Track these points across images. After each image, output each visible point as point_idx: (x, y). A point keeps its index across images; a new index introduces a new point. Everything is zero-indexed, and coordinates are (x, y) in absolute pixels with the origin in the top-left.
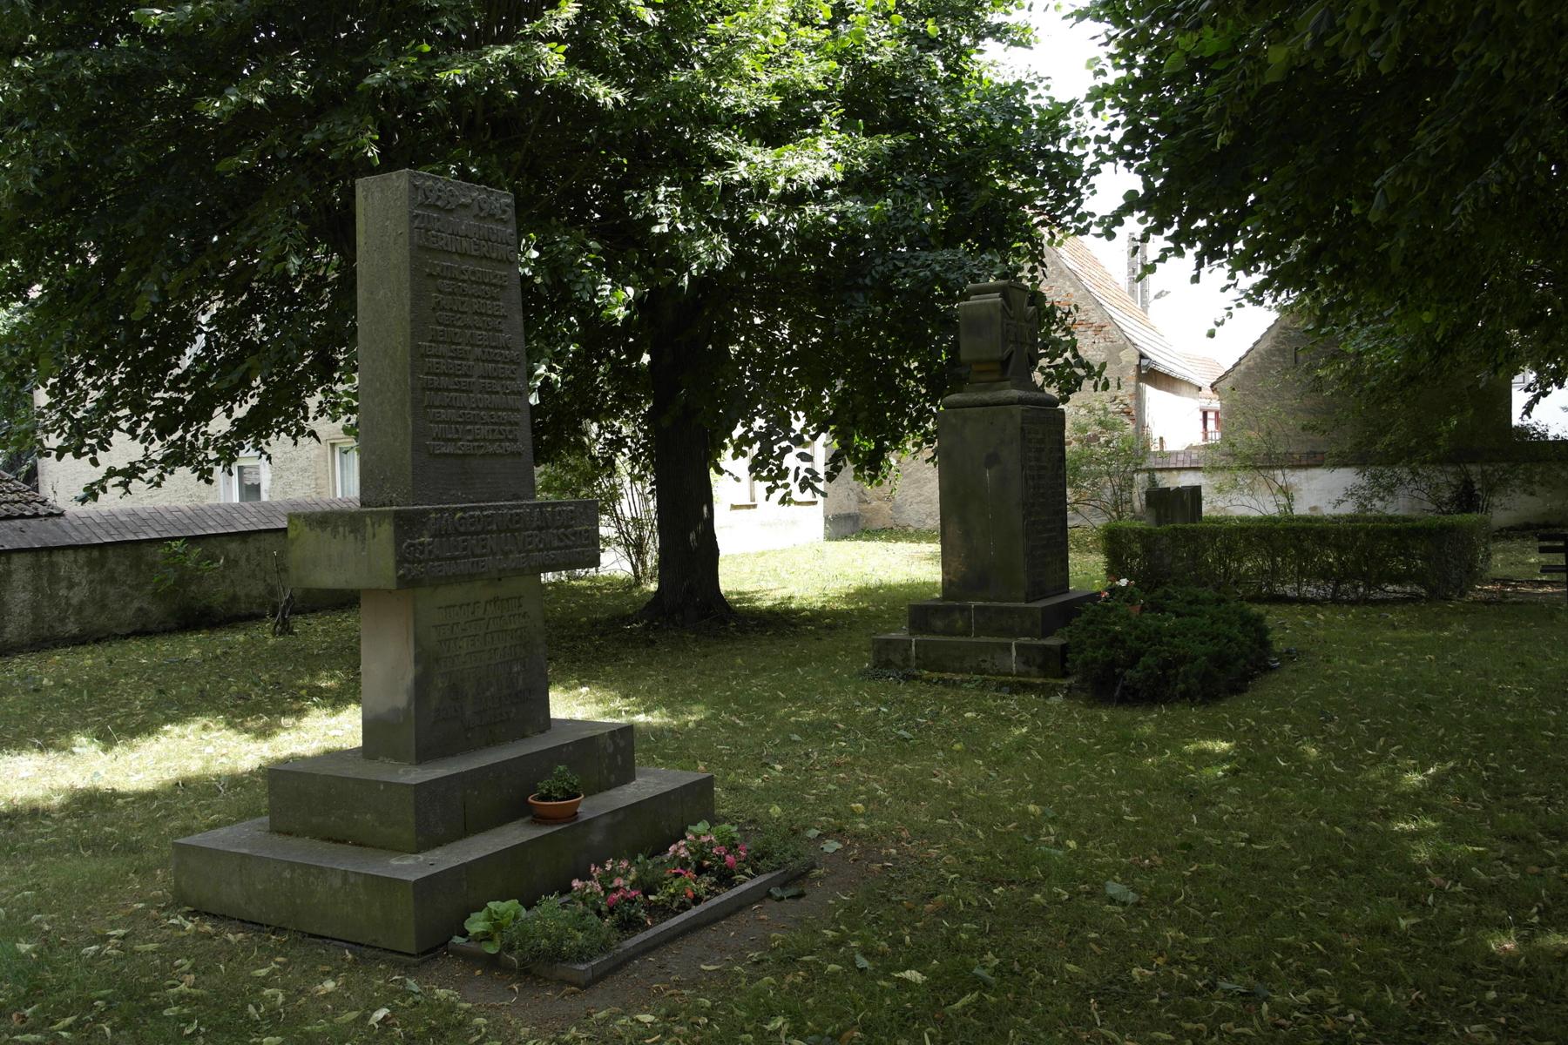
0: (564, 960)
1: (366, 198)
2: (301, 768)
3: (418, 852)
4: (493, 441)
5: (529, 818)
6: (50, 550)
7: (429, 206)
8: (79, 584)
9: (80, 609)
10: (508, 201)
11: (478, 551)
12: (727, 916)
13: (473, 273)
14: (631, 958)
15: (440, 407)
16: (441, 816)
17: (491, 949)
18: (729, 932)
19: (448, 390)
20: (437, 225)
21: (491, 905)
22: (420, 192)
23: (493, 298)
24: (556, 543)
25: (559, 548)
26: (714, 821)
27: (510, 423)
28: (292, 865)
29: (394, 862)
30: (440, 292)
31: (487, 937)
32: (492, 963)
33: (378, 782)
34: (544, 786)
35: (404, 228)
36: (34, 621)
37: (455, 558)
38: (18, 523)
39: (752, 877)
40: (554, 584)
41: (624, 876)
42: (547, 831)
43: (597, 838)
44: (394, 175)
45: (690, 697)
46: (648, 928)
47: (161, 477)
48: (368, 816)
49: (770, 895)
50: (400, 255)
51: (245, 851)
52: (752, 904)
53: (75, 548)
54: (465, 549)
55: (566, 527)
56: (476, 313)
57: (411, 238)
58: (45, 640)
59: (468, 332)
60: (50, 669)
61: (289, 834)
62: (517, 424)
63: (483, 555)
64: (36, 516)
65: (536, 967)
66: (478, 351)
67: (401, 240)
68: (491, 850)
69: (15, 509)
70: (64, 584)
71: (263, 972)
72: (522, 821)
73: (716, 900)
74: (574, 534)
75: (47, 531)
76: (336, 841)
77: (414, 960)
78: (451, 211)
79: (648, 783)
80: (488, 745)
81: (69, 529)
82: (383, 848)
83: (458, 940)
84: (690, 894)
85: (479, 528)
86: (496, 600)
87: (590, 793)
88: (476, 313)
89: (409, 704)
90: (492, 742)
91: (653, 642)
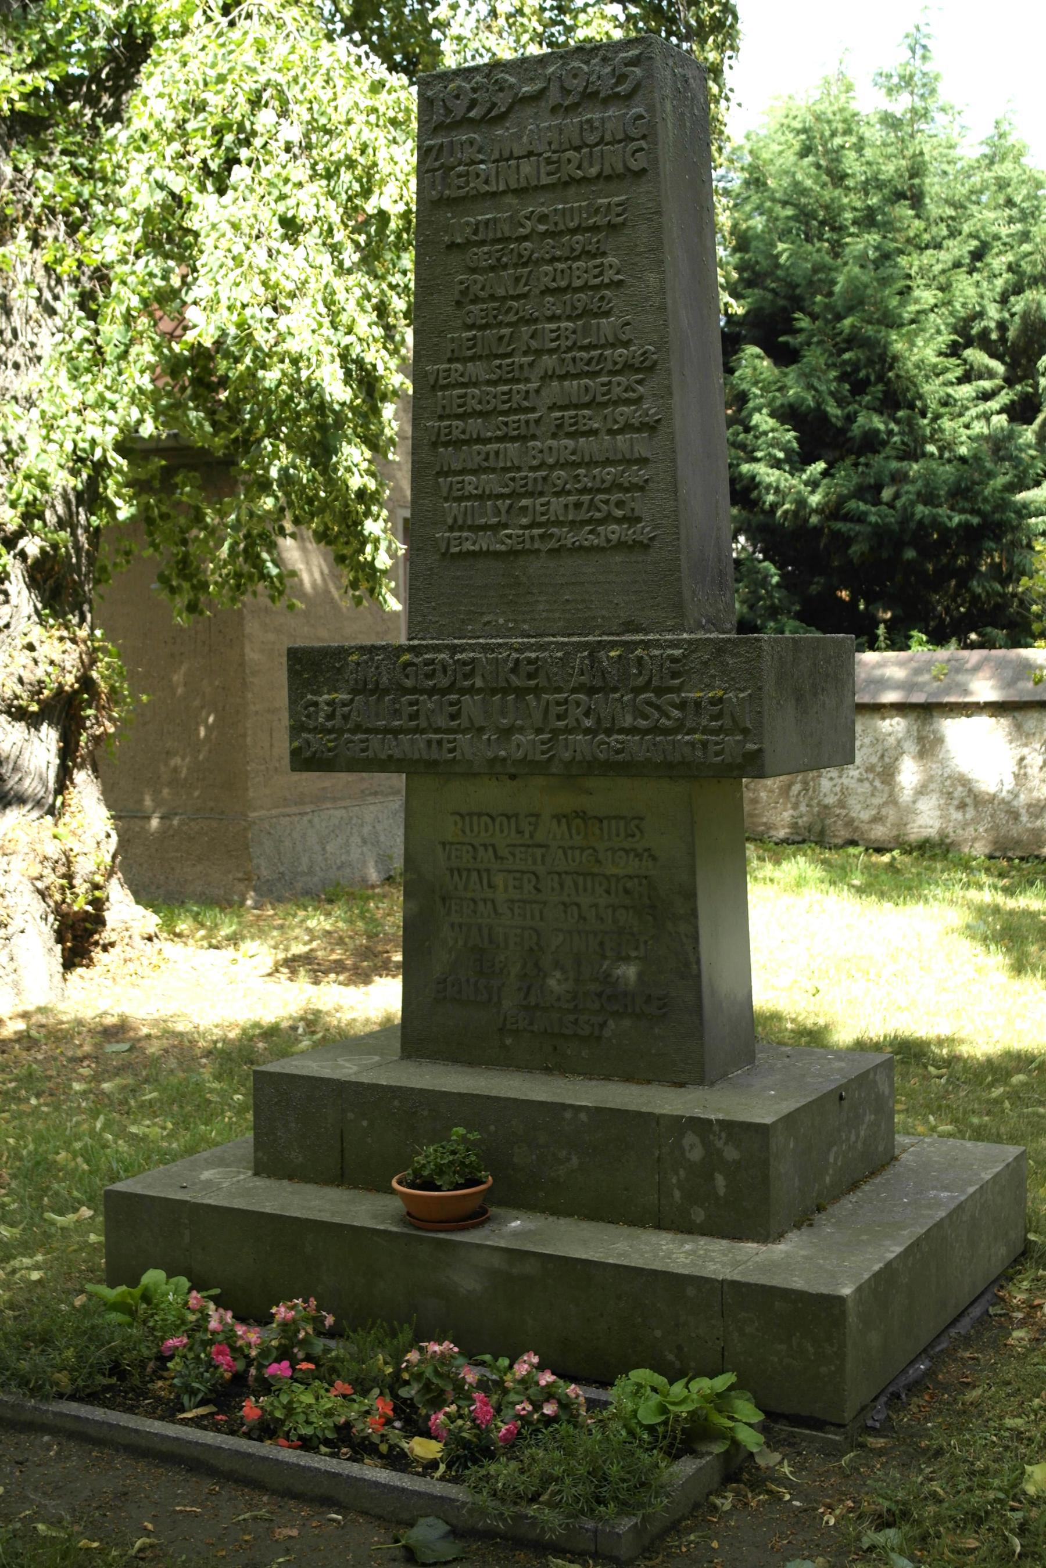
13: (543, 218)
15: (462, 472)
19: (480, 440)
23: (587, 254)
24: (628, 721)
25: (632, 731)
29: (622, 1246)
37: (396, 732)
54: (414, 716)
55: (660, 691)
56: (547, 291)
66: (548, 362)
74: (682, 706)
80: (547, 1070)
85: (445, 682)
88: (547, 291)
90: (556, 1065)
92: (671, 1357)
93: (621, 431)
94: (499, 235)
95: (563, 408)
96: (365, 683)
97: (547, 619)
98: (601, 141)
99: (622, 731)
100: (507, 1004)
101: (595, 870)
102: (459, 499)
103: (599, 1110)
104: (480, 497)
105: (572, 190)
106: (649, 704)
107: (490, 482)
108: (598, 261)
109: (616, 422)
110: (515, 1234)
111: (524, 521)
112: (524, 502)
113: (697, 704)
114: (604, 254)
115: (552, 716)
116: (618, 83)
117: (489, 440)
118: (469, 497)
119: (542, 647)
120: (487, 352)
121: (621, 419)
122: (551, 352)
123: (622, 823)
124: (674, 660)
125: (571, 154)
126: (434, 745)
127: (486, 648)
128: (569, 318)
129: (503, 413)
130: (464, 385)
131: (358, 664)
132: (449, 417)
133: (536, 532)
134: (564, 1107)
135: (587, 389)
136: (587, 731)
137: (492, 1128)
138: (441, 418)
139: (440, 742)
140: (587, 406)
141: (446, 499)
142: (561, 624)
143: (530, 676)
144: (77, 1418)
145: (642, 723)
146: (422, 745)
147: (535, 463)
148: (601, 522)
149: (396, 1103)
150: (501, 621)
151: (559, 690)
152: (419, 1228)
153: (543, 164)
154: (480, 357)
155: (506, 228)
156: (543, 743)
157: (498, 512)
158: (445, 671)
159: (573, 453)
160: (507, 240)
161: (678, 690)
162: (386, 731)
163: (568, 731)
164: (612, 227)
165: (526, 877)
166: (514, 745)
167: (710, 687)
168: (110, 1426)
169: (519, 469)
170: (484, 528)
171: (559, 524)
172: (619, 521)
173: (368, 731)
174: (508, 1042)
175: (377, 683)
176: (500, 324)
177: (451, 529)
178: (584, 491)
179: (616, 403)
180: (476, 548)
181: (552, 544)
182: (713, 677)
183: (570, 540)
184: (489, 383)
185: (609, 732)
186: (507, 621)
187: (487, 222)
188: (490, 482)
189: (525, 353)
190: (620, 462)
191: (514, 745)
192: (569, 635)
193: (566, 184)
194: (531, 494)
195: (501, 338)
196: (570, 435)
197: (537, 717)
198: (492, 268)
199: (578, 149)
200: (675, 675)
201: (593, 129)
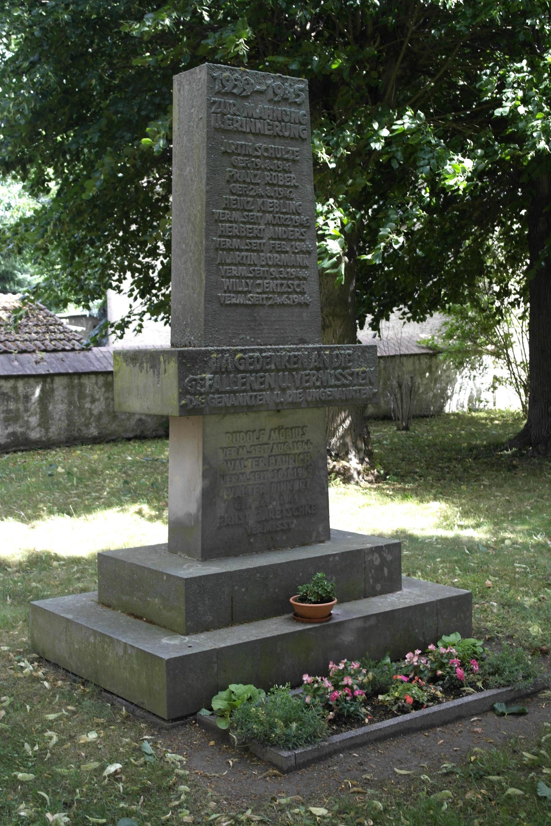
0: (273, 745)
1: (179, 91)
2: (110, 555)
3: (187, 634)
4: (281, 294)
5: (291, 615)
6: (79, 375)
7: (226, 94)
8: (99, 400)
9: (99, 417)
10: (302, 86)
11: (256, 386)
12: (444, 723)
13: (266, 150)
14: (336, 752)
15: (231, 264)
16: (207, 605)
17: (222, 725)
18: (440, 739)
20: (233, 110)
21: (232, 687)
22: (218, 82)
23: (285, 171)
24: (333, 382)
26: (465, 635)
27: (298, 278)
28: (95, 632)
29: (165, 641)
30: (235, 167)
31: (222, 714)
32: (223, 737)
33: (163, 574)
34: (302, 589)
35: (203, 114)
36: (68, 425)
37: (234, 392)
38: (61, 355)
39: (478, 690)
40: (457, 414)
41: (353, 676)
42: (299, 628)
43: (347, 638)
44: (197, 69)
45: (520, 517)
46: (364, 725)
47: (141, 326)
48: (156, 600)
49: (493, 709)
50: (200, 136)
51: (70, 617)
52: (473, 715)
53: (96, 373)
54: (244, 384)
55: (344, 369)
56: (268, 184)
57: (208, 122)
58: (75, 439)
59: (260, 201)
60: (61, 461)
61: (109, 606)
62: (305, 279)
63: (261, 390)
64: (73, 350)
65: (252, 747)
66: (269, 217)
67: (201, 125)
68: (245, 639)
69: (60, 345)
70: (88, 399)
71: (52, 717)
72: (287, 616)
73: (436, 708)
74: (352, 374)
75: (79, 361)
76: (136, 617)
77: (166, 724)
78: (247, 97)
79: (413, 592)
81: (94, 360)
82: (165, 627)
83: (204, 712)
84: (410, 700)
85: (258, 367)
86: (279, 428)
87: (346, 597)
88: (268, 184)
89: (198, 511)
90: (273, 546)
91: (515, 467)
92: (421, 638)
93: (298, 253)
94: (247, 153)
95: (274, 239)
96: (221, 368)
97: (268, 337)
98: (289, 121)
99: (331, 386)
100: (251, 522)
101: (288, 452)
102: (229, 278)
103: (343, 553)
104: (238, 277)
105: (277, 140)
106: (341, 374)
107: (243, 270)
108: (289, 175)
109: (296, 249)
111: (259, 290)
112: (258, 281)
113: (358, 373)
114: (290, 172)
115: (304, 381)
116: (296, 98)
117: (242, 250)
118: (235, 277)
119: (298, 350)
120: (242, 208)
121: (298, 247)
122: (270, 212)
123: (300, 429)
124: (349, 355)
125: (277, 123)
126: (253, 398)
127: (275, 350)
128: (277, 198)
129: (250, 238)
130: (231, 222)
131: (217, 358)
132: (224, 237)
133: (265, 296)
134: (329, 556)
135: (285, 232)
136: (318, 387)
137: (301, 574)
138: (220, 236)
139: (256, 396)
140: (284, 240)
141: (223, 277)
142: (274, 339)
143: (295, 363)
144: (352, 738)
145: (338, 383)
146: (248, 398)
147: (264, 263)
148: (290, 293)
149: (258, 575)
150: (248, 338)
151: (305, 369)
152: (321, 622)
153: (266, 124)
154: (238, 210)
155: (250, 150)
156: (300, 394)
157: (247, 284)
158: (258, 362)
159: (280, 261)
160: (249, 155)
161: (349, 368)
162: (230, 392)
163: (309, 388)
164: (294, 161)
165: (260, 460)
166: (288, 395)
167: (361, 366)
168: (368, 733)
169: (256, 265)
170: (240, 292)
171: (273, 292)
172: (297, 293)
173: (222, 393)
174: (252, 540)
175: (226, 368)
176: (247, 195)
177: (225, 292)
178: (284, 278)
179: (295, 240)
180: (238, 302)
181: (270, 302)
182: (361, 362)
183: (279, 300)
184: (243, 223)
185: (325, 387)
186: (251, 338)
187: (242, 145)
188: (243, 270)
189: (258, 211)
190: (297, 267)
191: (288, 395)
192: (278, 345)
193: (275, 136)
194: (261, 278)
195: (248, 202)
196: (278, 252)
197: (298, 383)
198: (243, 168)
199: (280, 122)
200: (350, 361)
201: (286, 115)
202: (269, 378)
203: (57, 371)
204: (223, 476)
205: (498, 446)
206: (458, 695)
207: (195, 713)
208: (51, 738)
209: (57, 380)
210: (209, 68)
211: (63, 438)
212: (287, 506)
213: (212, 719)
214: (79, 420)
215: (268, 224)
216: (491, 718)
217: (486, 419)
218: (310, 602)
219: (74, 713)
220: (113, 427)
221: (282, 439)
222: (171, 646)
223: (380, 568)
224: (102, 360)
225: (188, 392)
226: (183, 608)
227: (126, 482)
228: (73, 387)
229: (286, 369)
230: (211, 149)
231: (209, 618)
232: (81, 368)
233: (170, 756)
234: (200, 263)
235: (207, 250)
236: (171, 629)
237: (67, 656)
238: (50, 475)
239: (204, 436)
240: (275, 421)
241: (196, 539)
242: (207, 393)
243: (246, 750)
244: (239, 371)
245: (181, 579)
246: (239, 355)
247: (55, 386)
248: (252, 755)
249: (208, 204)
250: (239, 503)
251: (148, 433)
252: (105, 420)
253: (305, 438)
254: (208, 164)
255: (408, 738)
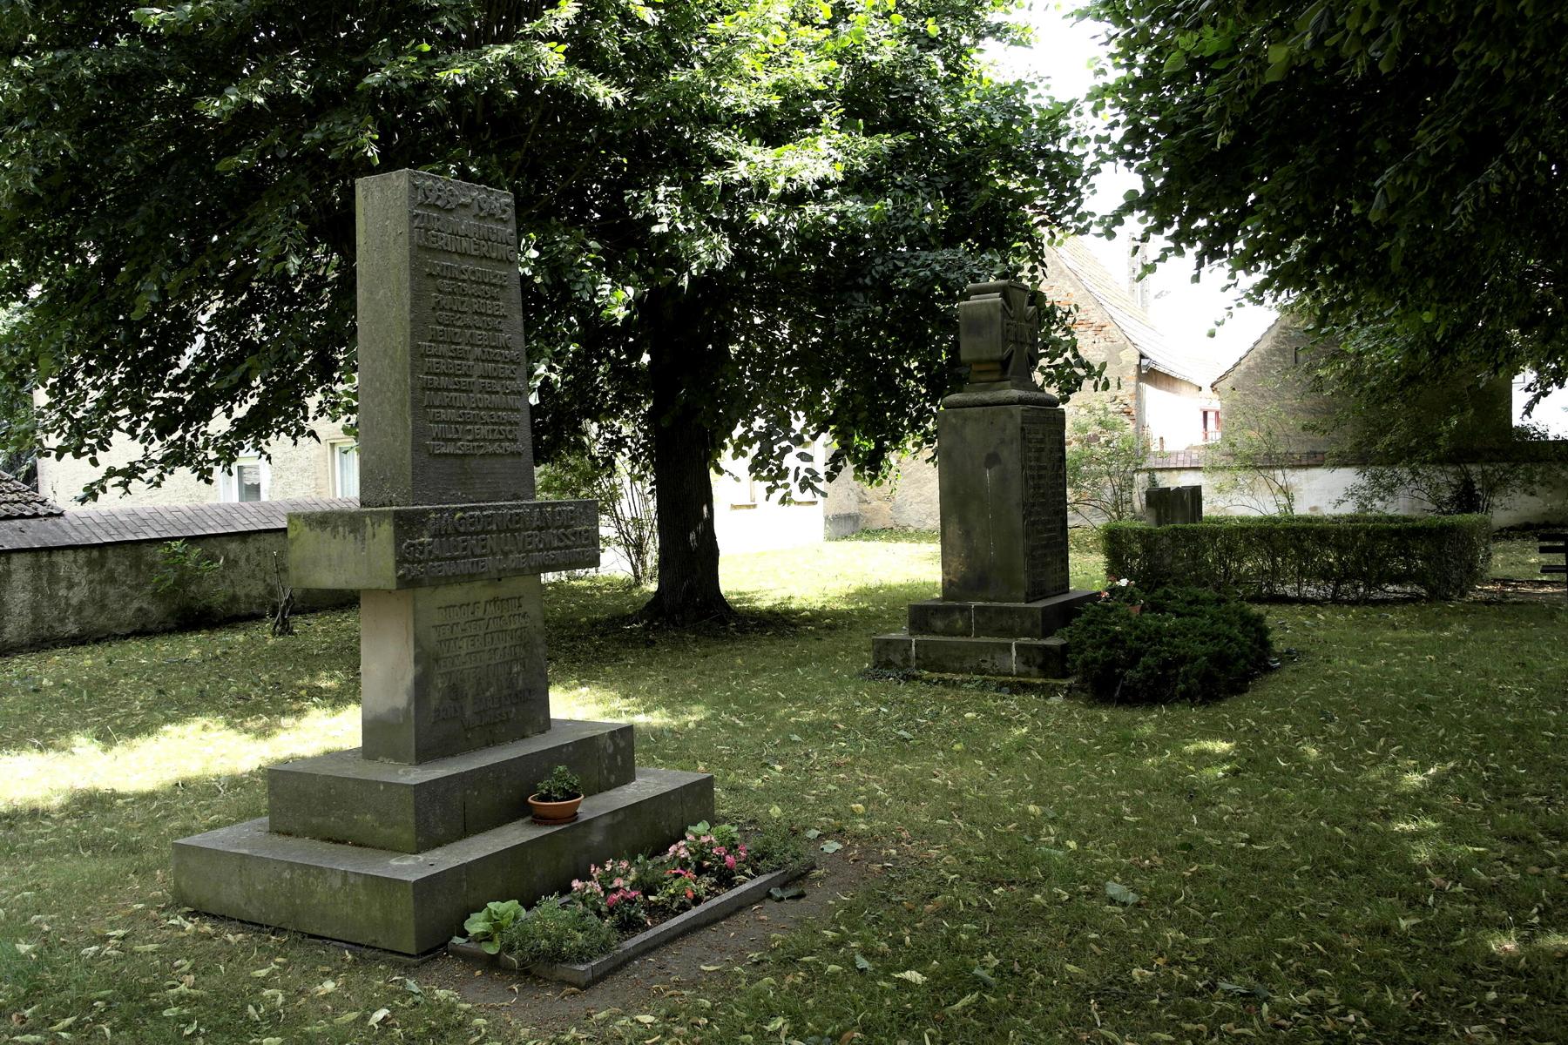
0: (564, 961)
2: (301, 768)
6: (49, 550)
7: (429, 206)
9: (80, 609)
11: (478, 551)
12: (727, 916)
13: (473, 272)
14: (631, 959)
16: (442, 816)
17: (491, 949)
18: (729, 932)
21: (491, 905)
23: (494, 298)
24: (556, 543)
26: (714, 822)
27: (510, 423)
29: (394, 862)
31: (487, 937)
33: (378, 783)
34: (543, 786)
36: (34, 622)
37: (455, 558)
38: (18, 523)
43: (597, 838)
45: (690, 697)
46: (648, 928)
47: (161, 477)
48: (368, 817)
49: (770, 896)
50: (399, 254)
51: (245, 851)
54: (465, 549)
55: (567, 527)
57: (411, 238)
58: (44, 640)
59: (468, 332)
60: (51, 668)
61: (289, 834)
64: (36, 516)
65: (536, 967)
66: (478, 351)
68: (491, 850)
69: (15, 510)
70: (63, 584)
73: (716, 901)
74: (574, 534)
77: (414, 960)
78: (451, 210)
79: (648, 783)
81: (69, 530)
83: (457, 940)
84: (690, 895)
85: (479, 528)
86: (495, 600)
90: (491, 742)
91: (653, 642)
100: (468, 713)
107: (451, 414)
110: (397, 869)
188: (451, 414)
202: (491, 541)
203: (15, 547)
204: (437, 661)
205: (626, 619)
206: (730, 885)
207: (446, 944)
208: (275, 997)
209: (15, 557)
210: (411, 175)
211: (25, 639)
212: (505, 692)
213: (472, 946)
214: (50, 614)
215: (477, 359)
216: (769, 903)
217: (591, 588)
218: (556, 800)
219: (285, 966)
220: (102, 620)
221: (498, 613)
222: (410, 868)
223: (613, 757)
224: (82, 528)
225: (406, 561)
226: (412, 820)
227: (160, 692)
228: (40, 568)
229: (508, 530)
230: (415, 271)
231: (441, 831)
232: (51, 542)
233: (441, 993)
234: (403, 406)
235: (413, 389)
236: (394, 848)
237: (242, 904)
238: (35, 691)
239: (415, 612)
240: (489, 593)
241: (409, 738)
242: (427, 561)
243: (527, 973)
244: (459, 534)
245: (407, 786)
246: (459, 515)
247: (13, 567)
248: (536, 978)
249: (412, 334)
250: (455, 692)
251: (151, 627)
252: (89, 611)
253: (522, 611)
254: (412, 288)
255: (696, 936)
